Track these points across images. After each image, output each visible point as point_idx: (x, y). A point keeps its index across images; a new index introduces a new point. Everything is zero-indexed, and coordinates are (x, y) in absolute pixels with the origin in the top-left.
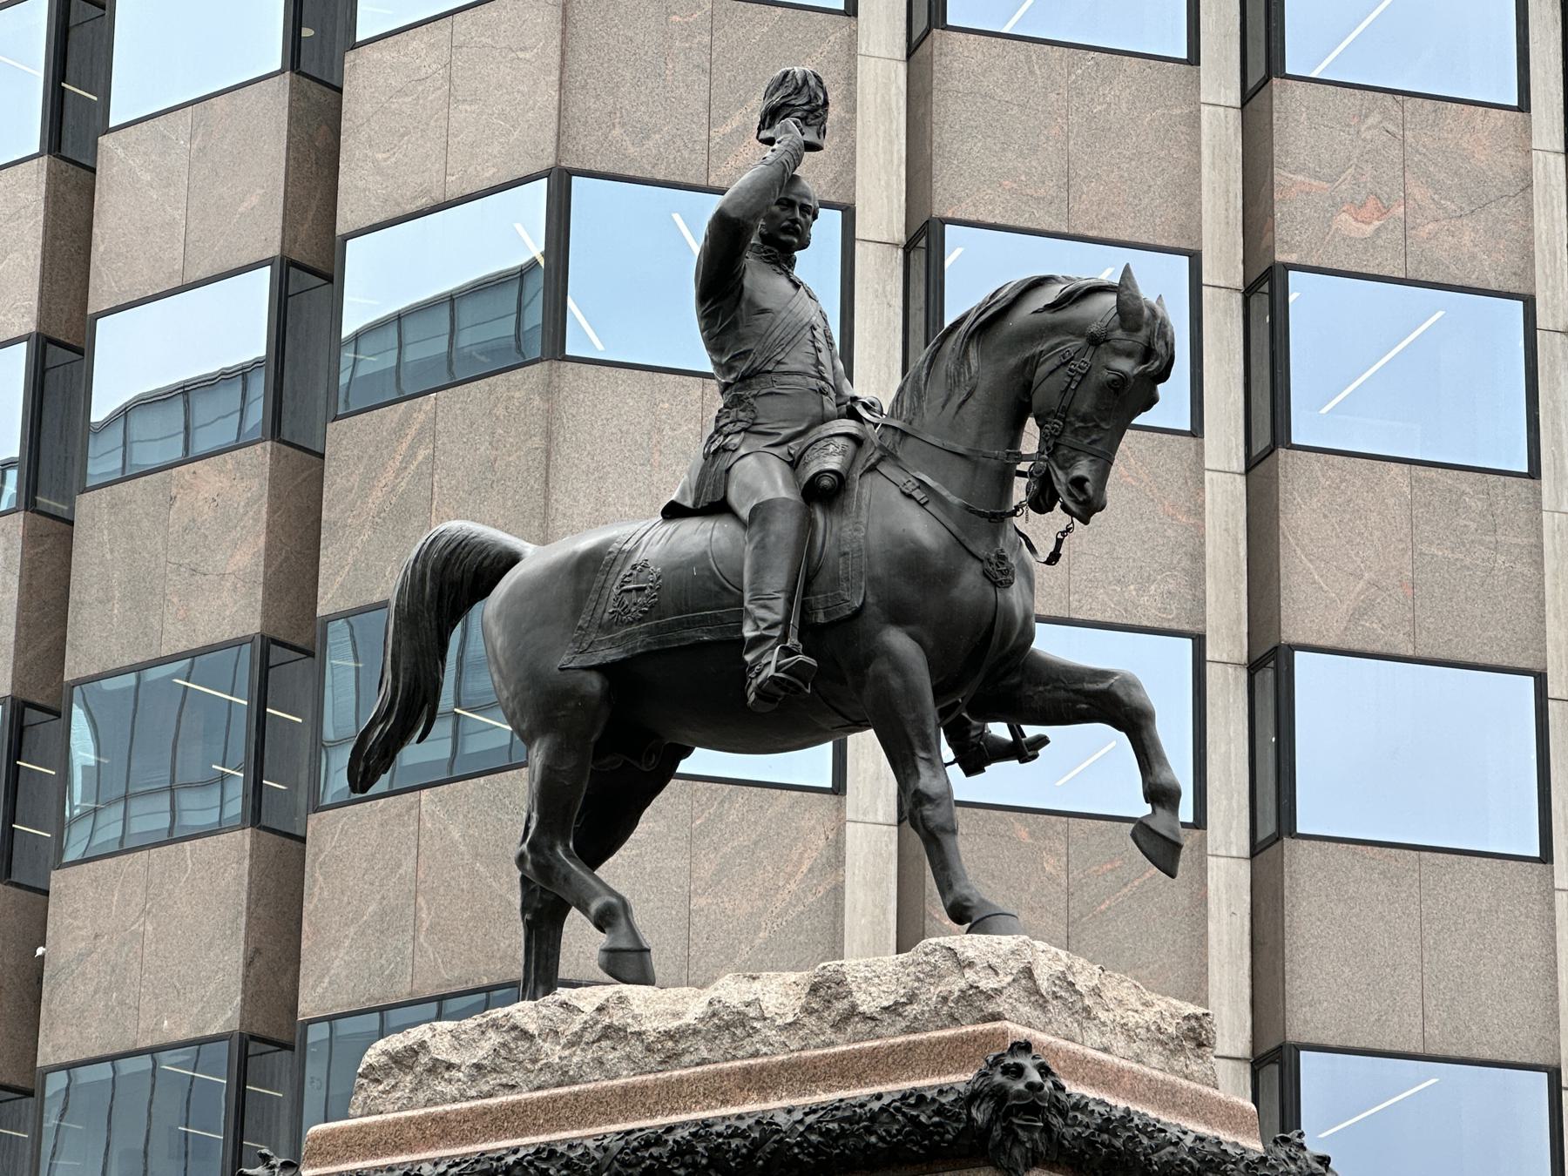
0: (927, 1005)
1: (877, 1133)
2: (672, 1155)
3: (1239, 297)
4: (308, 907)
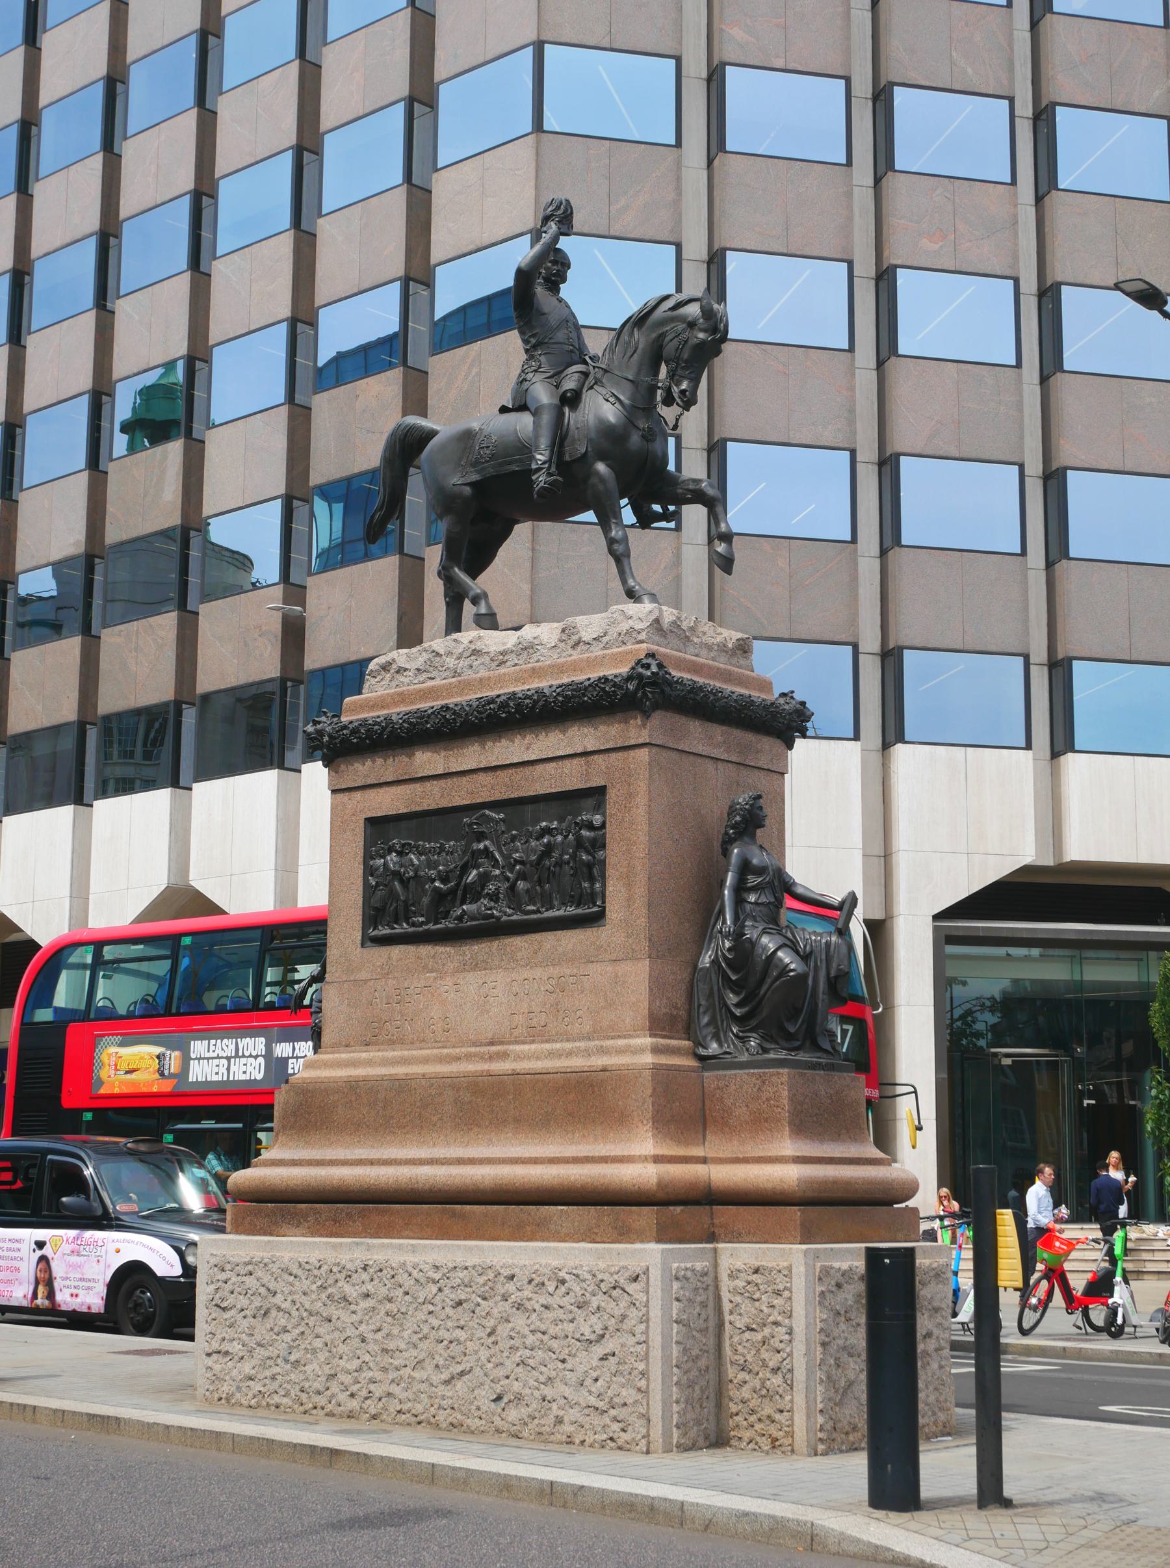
2: (499, 708)
3: (873, 282)
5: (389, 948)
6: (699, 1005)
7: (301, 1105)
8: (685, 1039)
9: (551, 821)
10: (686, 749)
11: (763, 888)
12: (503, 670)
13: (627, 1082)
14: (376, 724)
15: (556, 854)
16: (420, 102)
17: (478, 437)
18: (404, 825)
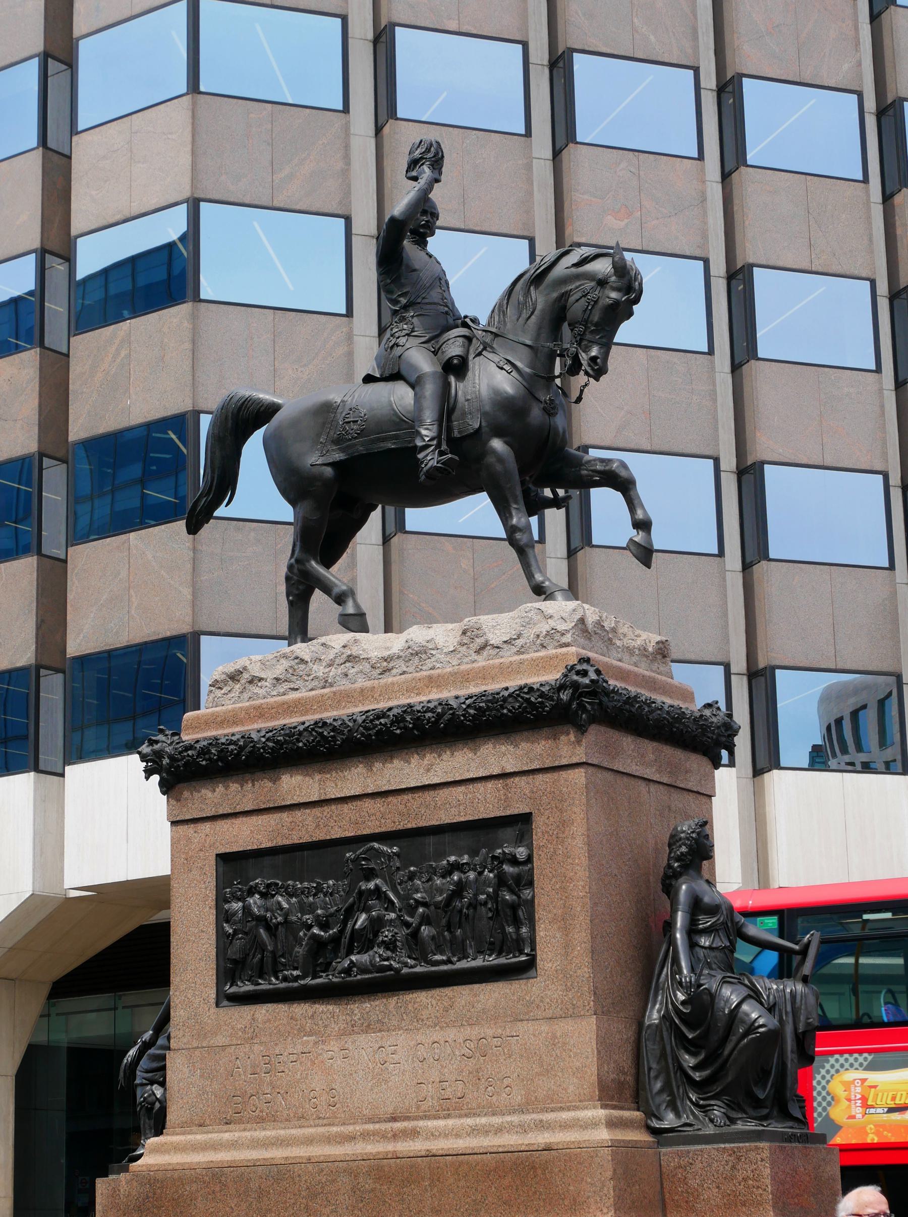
0: (528, 639)
1: (506, 708)
2: (392, 723)
4: (70, 597)
5: (253, 1008)
6: (650, 1069)
7: (148, 1197)
8: (634, 1110)
9: (460, 855)
10: (621, 769)
11: (717, 930)
12: (388, 679)
13: (579, 1163)
14: (231, 743)
15: (468, 895)
16: (55, 58)
17: (339, 410)
18: (267, 861)
